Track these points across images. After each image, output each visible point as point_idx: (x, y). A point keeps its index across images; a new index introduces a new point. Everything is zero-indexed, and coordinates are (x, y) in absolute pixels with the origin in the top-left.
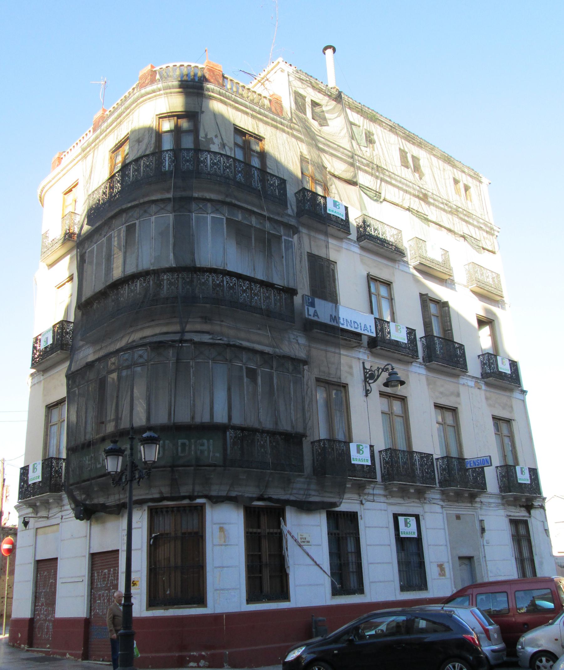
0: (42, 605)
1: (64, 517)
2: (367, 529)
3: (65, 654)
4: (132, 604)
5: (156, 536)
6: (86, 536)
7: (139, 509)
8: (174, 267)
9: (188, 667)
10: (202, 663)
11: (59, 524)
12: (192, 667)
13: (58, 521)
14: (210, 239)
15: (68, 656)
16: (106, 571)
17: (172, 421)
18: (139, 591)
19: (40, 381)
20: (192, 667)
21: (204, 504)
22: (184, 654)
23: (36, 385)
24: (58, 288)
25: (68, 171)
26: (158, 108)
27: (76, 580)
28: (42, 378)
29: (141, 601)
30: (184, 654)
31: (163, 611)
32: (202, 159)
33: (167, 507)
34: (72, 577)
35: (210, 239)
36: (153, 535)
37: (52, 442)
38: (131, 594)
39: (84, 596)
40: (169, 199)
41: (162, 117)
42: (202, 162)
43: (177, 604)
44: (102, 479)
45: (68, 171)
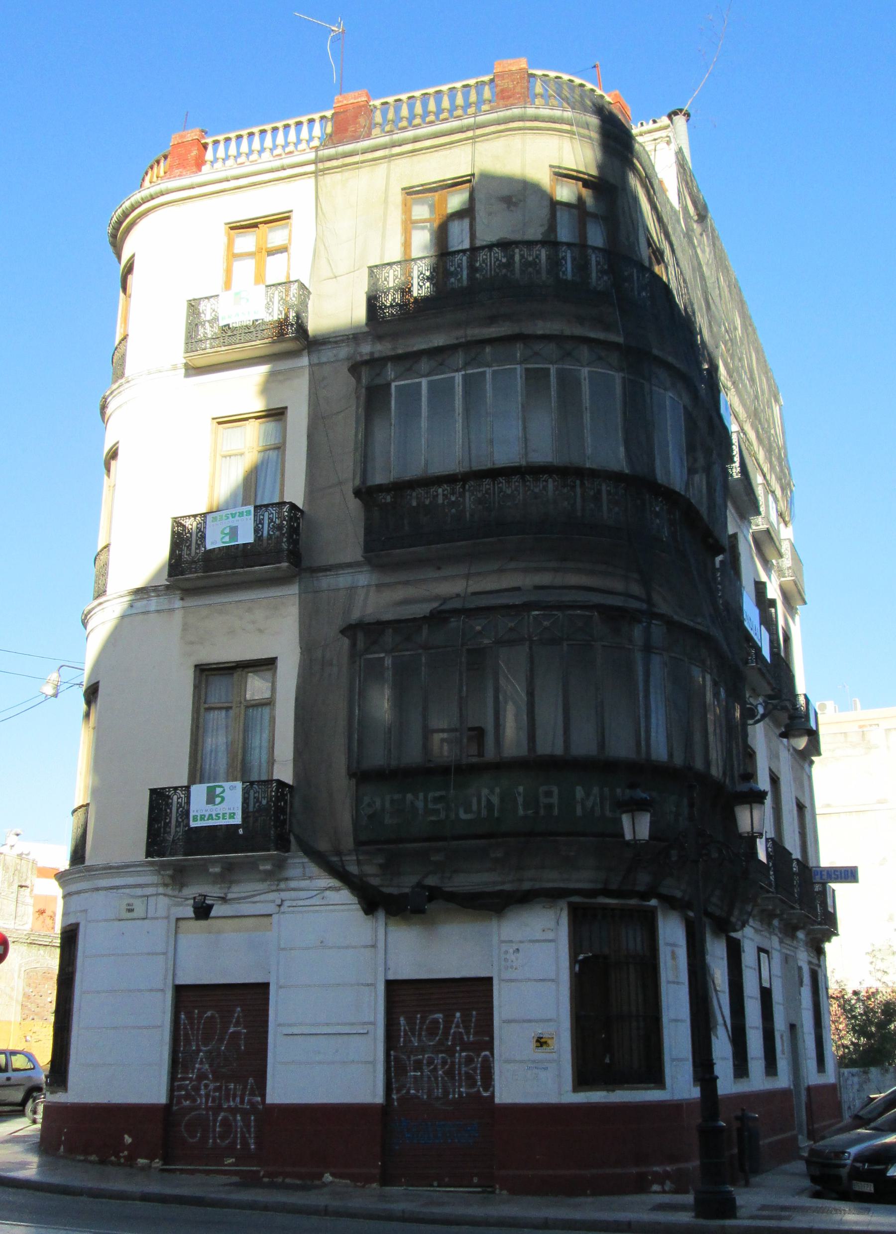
0: (202, 1076)
1: (286, 904)
2: (553, 976)
3: (320, 1176)
4: (717, 1077)
5: (585, 958)
6: (374, 946)
7: (551, 907)
8: (627, 475)
9: (651, 1192)
10: (668, 1186)
11: (271, 915)
12: (655, 1192)
13: (270, 908)
14: (424, 424)
15: (328, 1178)
16: (439, 1016)
17: (643, 755)
18: (554, 1056)
19: (172, 610)
20: (655, 1192)
21: (655, 908)
22: (643, 1169)
23: (153, 616)
24: (219, 423)
25: (254, 184)
26: (549, 156)
27: (346, 1029)
28: (178, 604)
29: (559, 1076)
30: (643, 1169)
31: (604, 1093)
32: (452, 269)
33: (605, 907)
34: (353, 1024)
35: (424, 424)
36: (581, 957)
37: (256, 742)
38: (712, 1060)
39: (373, 1063)
40: (617, 346)
41: (562, 175)
42: (452, 274)
43: (628, 1083)
44: (477, 842)
45: (254, 184)
